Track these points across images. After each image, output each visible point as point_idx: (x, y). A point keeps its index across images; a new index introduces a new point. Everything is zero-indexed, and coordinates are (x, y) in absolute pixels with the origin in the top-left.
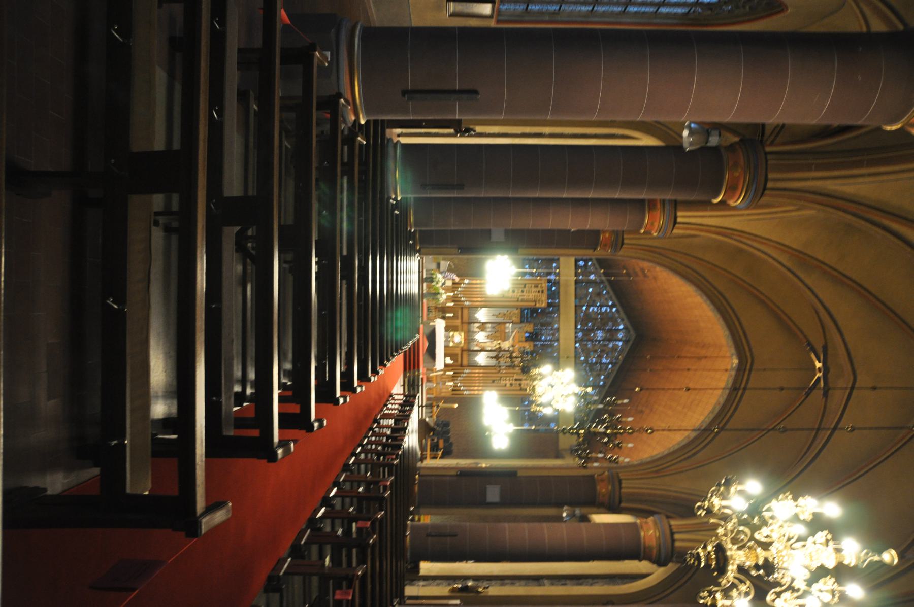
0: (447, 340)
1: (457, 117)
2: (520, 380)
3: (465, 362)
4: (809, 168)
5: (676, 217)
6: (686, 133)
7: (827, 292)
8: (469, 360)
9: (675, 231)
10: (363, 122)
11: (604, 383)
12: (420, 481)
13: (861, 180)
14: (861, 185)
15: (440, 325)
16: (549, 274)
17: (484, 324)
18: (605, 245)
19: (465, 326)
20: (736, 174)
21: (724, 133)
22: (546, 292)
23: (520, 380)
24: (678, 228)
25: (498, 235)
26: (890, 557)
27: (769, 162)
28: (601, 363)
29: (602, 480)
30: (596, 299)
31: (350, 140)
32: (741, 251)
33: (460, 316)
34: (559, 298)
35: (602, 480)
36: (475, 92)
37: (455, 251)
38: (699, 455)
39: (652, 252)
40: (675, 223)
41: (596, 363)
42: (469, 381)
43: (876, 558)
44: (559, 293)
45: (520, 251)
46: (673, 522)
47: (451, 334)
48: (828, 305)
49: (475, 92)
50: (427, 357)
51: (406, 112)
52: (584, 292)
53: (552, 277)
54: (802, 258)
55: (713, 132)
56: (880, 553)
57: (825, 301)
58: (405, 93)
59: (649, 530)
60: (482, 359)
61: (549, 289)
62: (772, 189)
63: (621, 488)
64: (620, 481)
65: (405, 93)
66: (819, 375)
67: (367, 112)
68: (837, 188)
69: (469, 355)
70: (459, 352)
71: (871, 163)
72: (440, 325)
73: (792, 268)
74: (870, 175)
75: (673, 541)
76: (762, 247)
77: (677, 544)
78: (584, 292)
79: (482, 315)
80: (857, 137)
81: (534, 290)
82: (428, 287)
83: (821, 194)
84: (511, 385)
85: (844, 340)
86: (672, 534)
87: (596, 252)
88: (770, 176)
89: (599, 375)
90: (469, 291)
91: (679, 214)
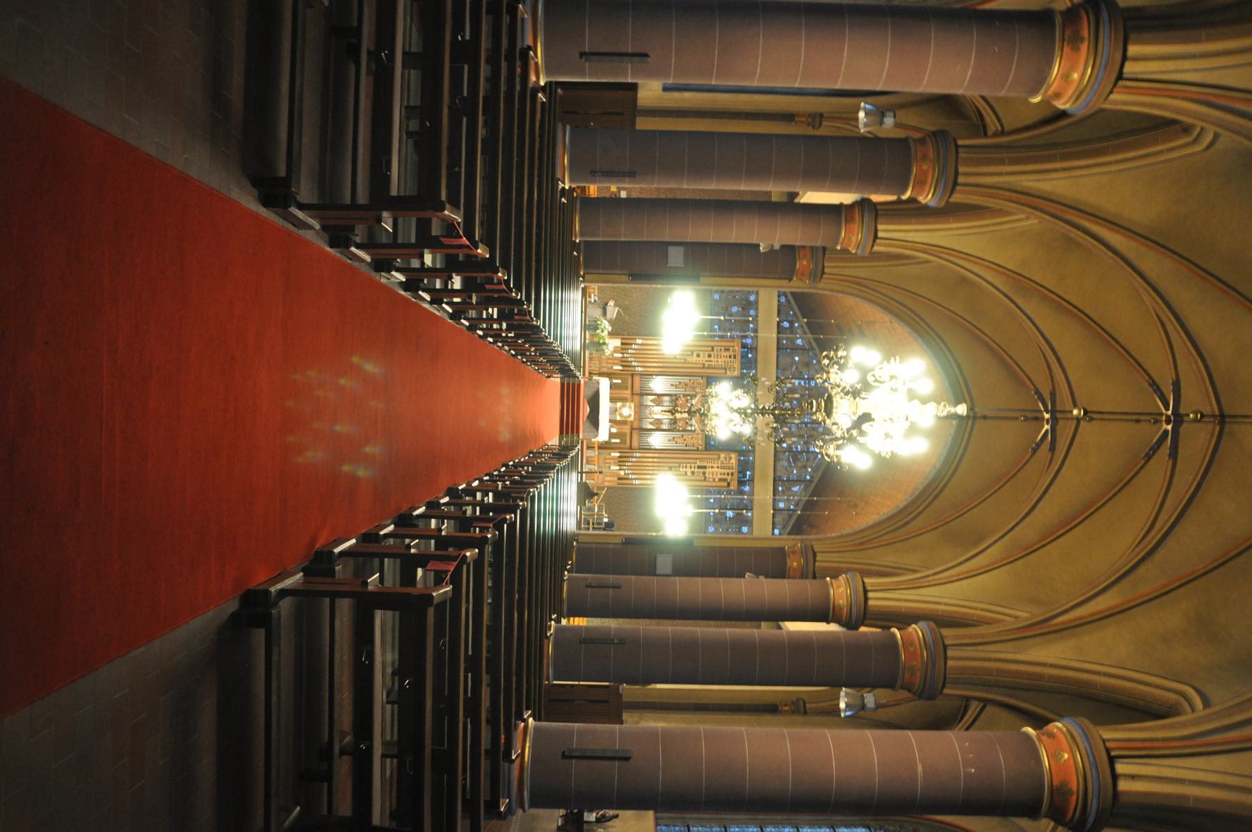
0: (614, 411)
1: (629, 81)
2: (705, 467)
3: (635, 444)
4: (1001, 162)
5: (876, 231)
6: (862, 115)
7: (1050, 322)
8: (640, 441)
9: (876, 248)
10: (542, 83)
11: (812, 477)
12: (579, 549)
13: (1054, 175)
14: (1058, 182)
15: (604, 385)
16: (746, 337)
17: (659, 395)
18: (803, 274)
19: (636, 398)
20: (925, 167)
21: (900, 113)
22: (739, 357)
23: (705, 467)
24: (880, 245)
25: (676, 257)
26: (962, 409)
27: (961, 155)
28: (808, 452)
29: (794, 553)
30: (804, 370)
31: (534, 97)
32: (963, 280)
33: (630, 383)
34: (756, 369)
35: (794, 553)
36: (646, 55)
37: (625, 278)
38: (910, 526)
39: (858, 284)
40: (876, 237)
41: (802, 452)
42: (640, 468)
43: (953, 410)
44: (756, 361)
45: (702, 279)
46: (867, 580)
47: (619, 404)
48: (1049, 338)
49: (646, 55)
50: (588, 424)
51: (583, 74)
52: (789, 360)
53: (749, 341)
54: (1018, 279)
55: (888, 114)
56: (956, 405)
57: (1045, 333)
58: (582, 54)
59: (839, 587)
60: (657, 440)
61: (744, 356)
62: (964, 185)
63: (815, 560)
64: (815, 554)
65: (582, 54)
66: (1047, 427)
67: (548, 73)
68: (1032, 184)
69: (640, 435)
70: (628, 432)
71: (1064, 157)
72: (604, 385)
73: (1009, 294)
74: (1064, 169)
75: (866, 599)
76: (976, 269)
77: (871, 603)
78: (789, 360)
79: (659, 385)
80: (1057, 130)
81: (724, 353)
82: (592, 336)
83: (1010, 190)
84: (693, 473)
85: (1067, 378)
86: (866, 591)
87: (792, 284)
88: (961, 169)
89: (805, 467)
90: (642, 355)
91: (880, 227)
